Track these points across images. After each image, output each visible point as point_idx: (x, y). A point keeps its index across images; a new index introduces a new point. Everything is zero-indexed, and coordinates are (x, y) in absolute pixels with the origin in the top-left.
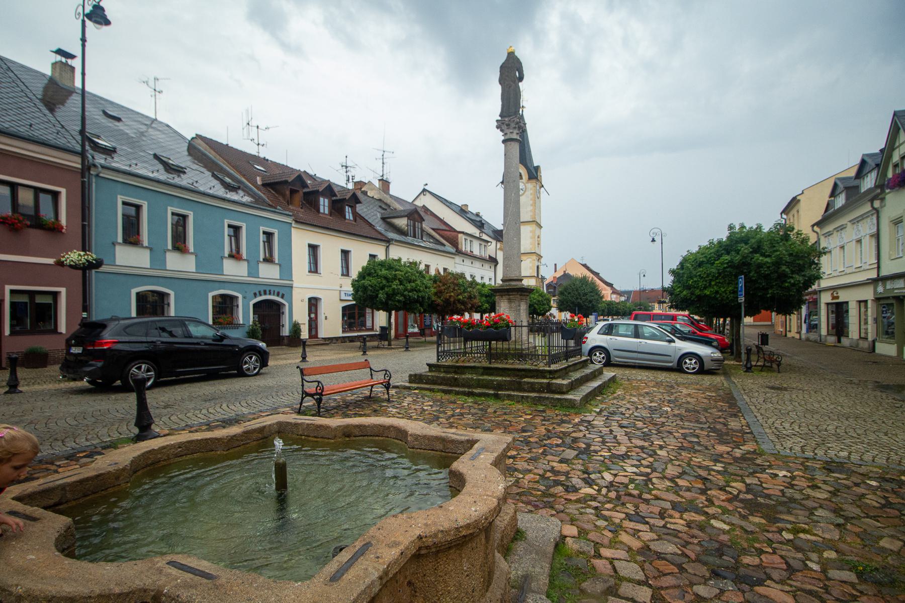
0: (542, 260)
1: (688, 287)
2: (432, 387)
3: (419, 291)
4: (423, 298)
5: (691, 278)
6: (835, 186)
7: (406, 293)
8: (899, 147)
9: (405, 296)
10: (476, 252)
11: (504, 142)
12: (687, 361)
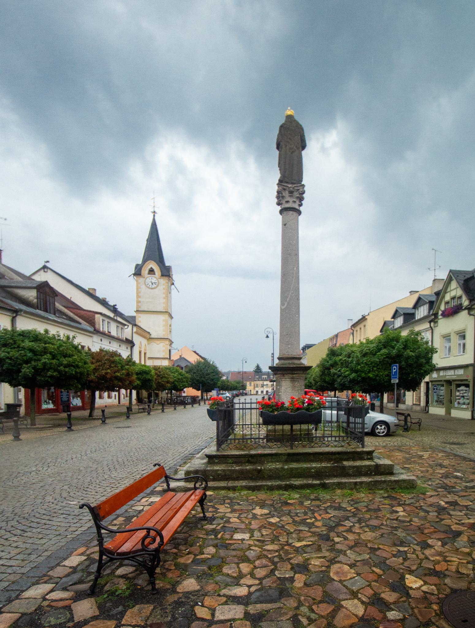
0: (173, 345)
1: (356, 371)
2: (231, 484)
3: (77, 366)
4: (81, 373)
5: (359, 364)
6: (396, 311)
7: (62, 368)
8: (451, 291)
9: (59, 372)
10: (114, 333)
11: (281, 212)
12: (379, 427)
